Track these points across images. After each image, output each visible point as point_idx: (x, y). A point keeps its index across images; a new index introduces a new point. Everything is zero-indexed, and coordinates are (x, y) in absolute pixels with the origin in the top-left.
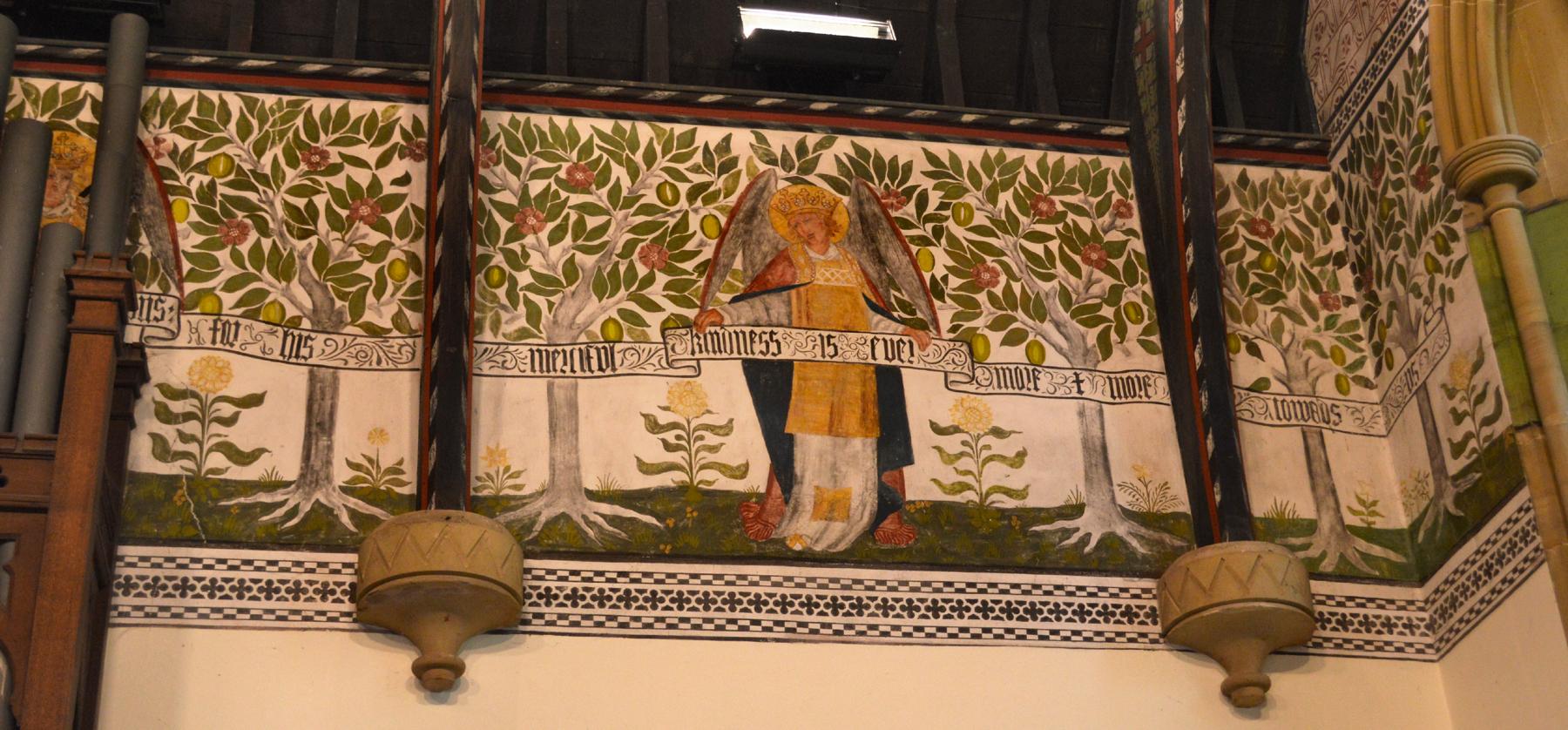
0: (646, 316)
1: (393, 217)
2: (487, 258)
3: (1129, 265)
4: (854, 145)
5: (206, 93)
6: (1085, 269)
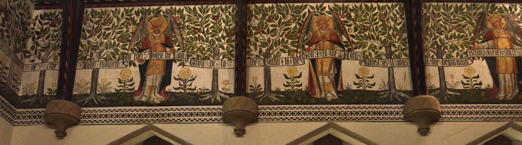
2: (249, 40)
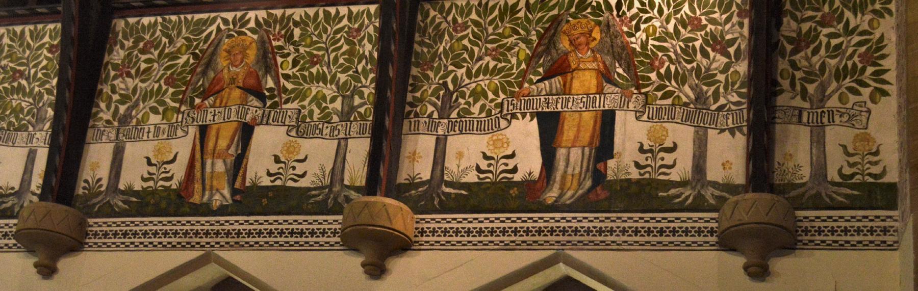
0: (861, 89)
1: (732, 50)
3: (738, 51)
4: (344, 16)
5: (327, 8)
6: (712, 54)
